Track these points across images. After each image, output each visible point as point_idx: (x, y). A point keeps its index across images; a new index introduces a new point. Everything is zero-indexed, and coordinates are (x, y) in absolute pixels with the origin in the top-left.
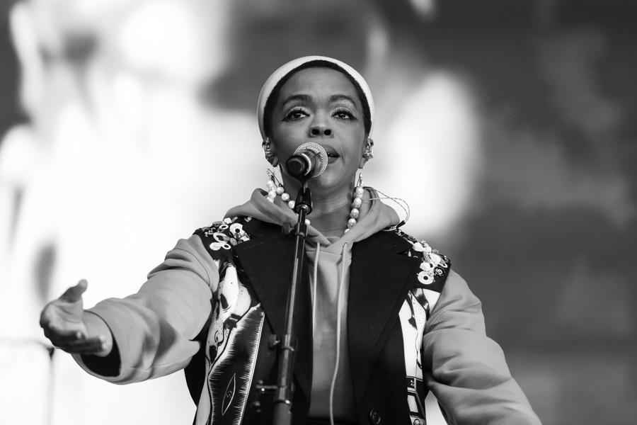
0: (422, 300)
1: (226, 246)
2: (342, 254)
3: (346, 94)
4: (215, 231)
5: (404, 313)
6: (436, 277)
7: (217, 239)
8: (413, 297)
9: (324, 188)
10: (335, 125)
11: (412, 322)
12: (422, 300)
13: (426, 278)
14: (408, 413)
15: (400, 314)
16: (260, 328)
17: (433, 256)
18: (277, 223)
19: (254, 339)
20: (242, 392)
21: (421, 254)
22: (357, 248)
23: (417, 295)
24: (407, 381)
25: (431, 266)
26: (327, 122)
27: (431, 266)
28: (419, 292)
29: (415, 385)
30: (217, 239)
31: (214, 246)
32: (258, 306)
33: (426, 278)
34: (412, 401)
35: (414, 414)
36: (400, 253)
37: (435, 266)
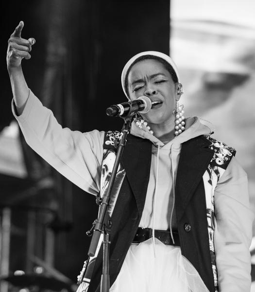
0: (217, 172)
1: (113, 144)
2: (171, 150)
3: (157, 72)
4: (112, 136)
5: (206, 177)
6: (225, 161)
7: (111, 139)
8: (213, 171)
9: (20, 109)
10: (156, 87)
11: (210, 182)
12: (217, 172)
13: (220, 161)
14: (207, 225)
15: (203, 177)
16: (122, 181)
17: (224, 150)
18: (140, 136)
19: (118, 187)
20: (109, 211)
21: (218, 149)
22: (184, 145)
23: (214, 169)
24: (207, 211)
25: (223, 155)
26: (153, 88)
27: (223, 155)
28: (216, 168)
29: (211, 213)
30: (111, 139)
31: (107, 143)
32: (123, 170)
33: (220, 161)
34: (209, 220)
35: (210, 227)
36: (205, 147)
37: (225, 155)
